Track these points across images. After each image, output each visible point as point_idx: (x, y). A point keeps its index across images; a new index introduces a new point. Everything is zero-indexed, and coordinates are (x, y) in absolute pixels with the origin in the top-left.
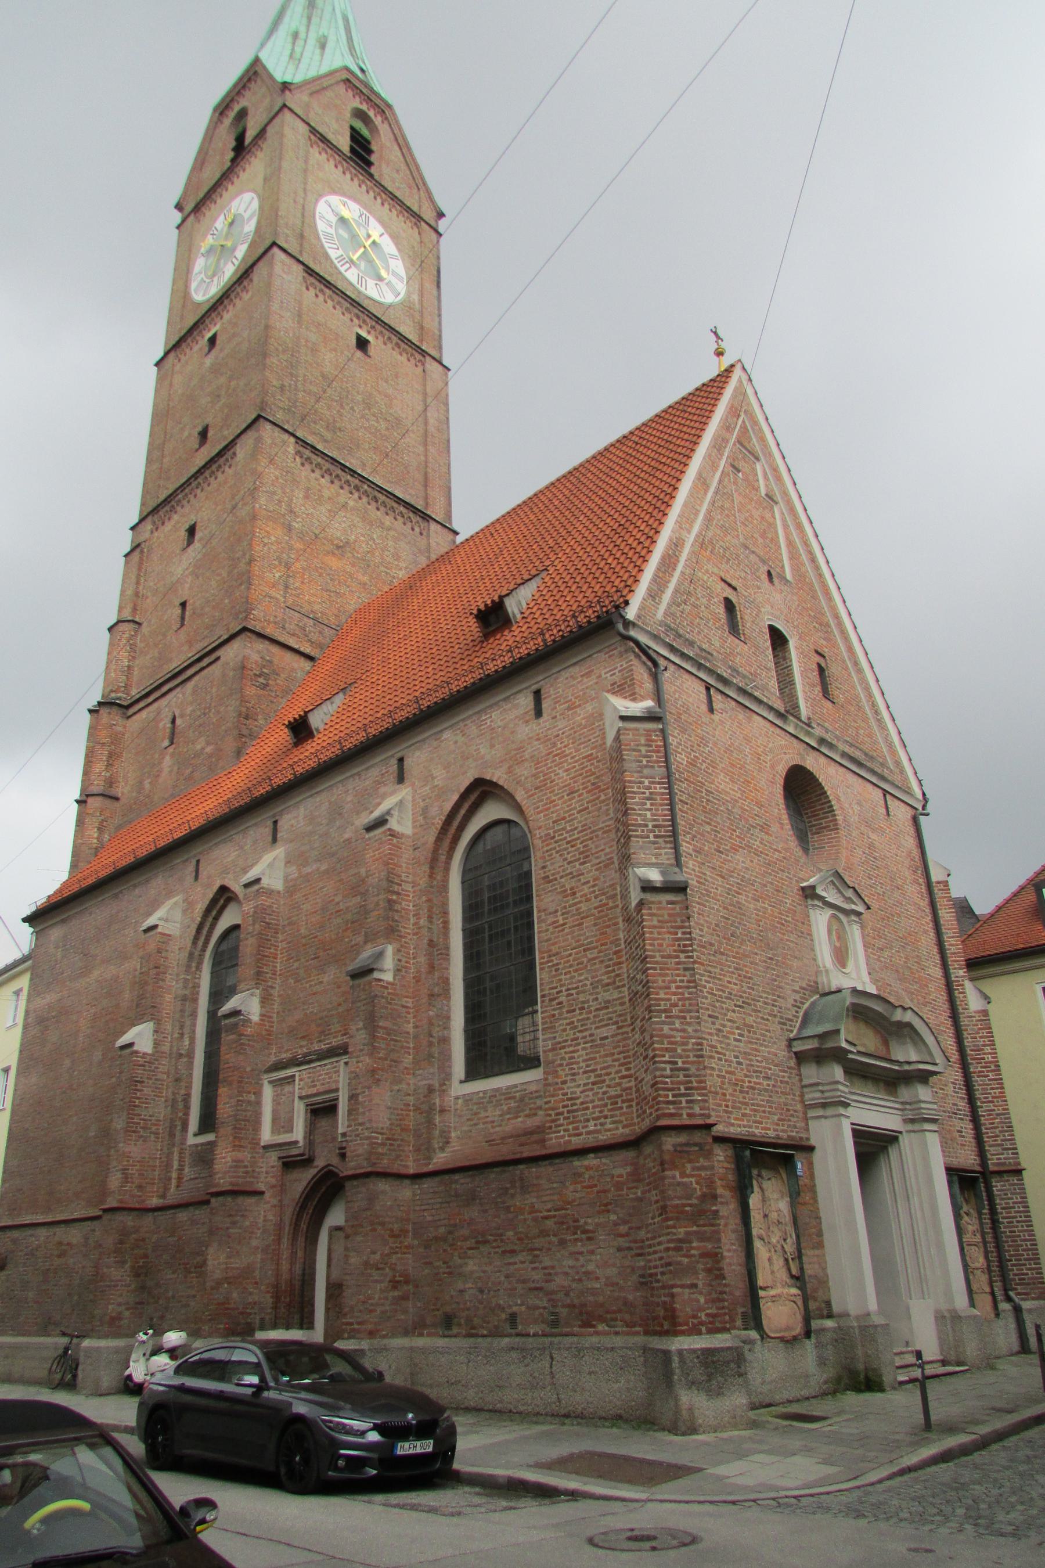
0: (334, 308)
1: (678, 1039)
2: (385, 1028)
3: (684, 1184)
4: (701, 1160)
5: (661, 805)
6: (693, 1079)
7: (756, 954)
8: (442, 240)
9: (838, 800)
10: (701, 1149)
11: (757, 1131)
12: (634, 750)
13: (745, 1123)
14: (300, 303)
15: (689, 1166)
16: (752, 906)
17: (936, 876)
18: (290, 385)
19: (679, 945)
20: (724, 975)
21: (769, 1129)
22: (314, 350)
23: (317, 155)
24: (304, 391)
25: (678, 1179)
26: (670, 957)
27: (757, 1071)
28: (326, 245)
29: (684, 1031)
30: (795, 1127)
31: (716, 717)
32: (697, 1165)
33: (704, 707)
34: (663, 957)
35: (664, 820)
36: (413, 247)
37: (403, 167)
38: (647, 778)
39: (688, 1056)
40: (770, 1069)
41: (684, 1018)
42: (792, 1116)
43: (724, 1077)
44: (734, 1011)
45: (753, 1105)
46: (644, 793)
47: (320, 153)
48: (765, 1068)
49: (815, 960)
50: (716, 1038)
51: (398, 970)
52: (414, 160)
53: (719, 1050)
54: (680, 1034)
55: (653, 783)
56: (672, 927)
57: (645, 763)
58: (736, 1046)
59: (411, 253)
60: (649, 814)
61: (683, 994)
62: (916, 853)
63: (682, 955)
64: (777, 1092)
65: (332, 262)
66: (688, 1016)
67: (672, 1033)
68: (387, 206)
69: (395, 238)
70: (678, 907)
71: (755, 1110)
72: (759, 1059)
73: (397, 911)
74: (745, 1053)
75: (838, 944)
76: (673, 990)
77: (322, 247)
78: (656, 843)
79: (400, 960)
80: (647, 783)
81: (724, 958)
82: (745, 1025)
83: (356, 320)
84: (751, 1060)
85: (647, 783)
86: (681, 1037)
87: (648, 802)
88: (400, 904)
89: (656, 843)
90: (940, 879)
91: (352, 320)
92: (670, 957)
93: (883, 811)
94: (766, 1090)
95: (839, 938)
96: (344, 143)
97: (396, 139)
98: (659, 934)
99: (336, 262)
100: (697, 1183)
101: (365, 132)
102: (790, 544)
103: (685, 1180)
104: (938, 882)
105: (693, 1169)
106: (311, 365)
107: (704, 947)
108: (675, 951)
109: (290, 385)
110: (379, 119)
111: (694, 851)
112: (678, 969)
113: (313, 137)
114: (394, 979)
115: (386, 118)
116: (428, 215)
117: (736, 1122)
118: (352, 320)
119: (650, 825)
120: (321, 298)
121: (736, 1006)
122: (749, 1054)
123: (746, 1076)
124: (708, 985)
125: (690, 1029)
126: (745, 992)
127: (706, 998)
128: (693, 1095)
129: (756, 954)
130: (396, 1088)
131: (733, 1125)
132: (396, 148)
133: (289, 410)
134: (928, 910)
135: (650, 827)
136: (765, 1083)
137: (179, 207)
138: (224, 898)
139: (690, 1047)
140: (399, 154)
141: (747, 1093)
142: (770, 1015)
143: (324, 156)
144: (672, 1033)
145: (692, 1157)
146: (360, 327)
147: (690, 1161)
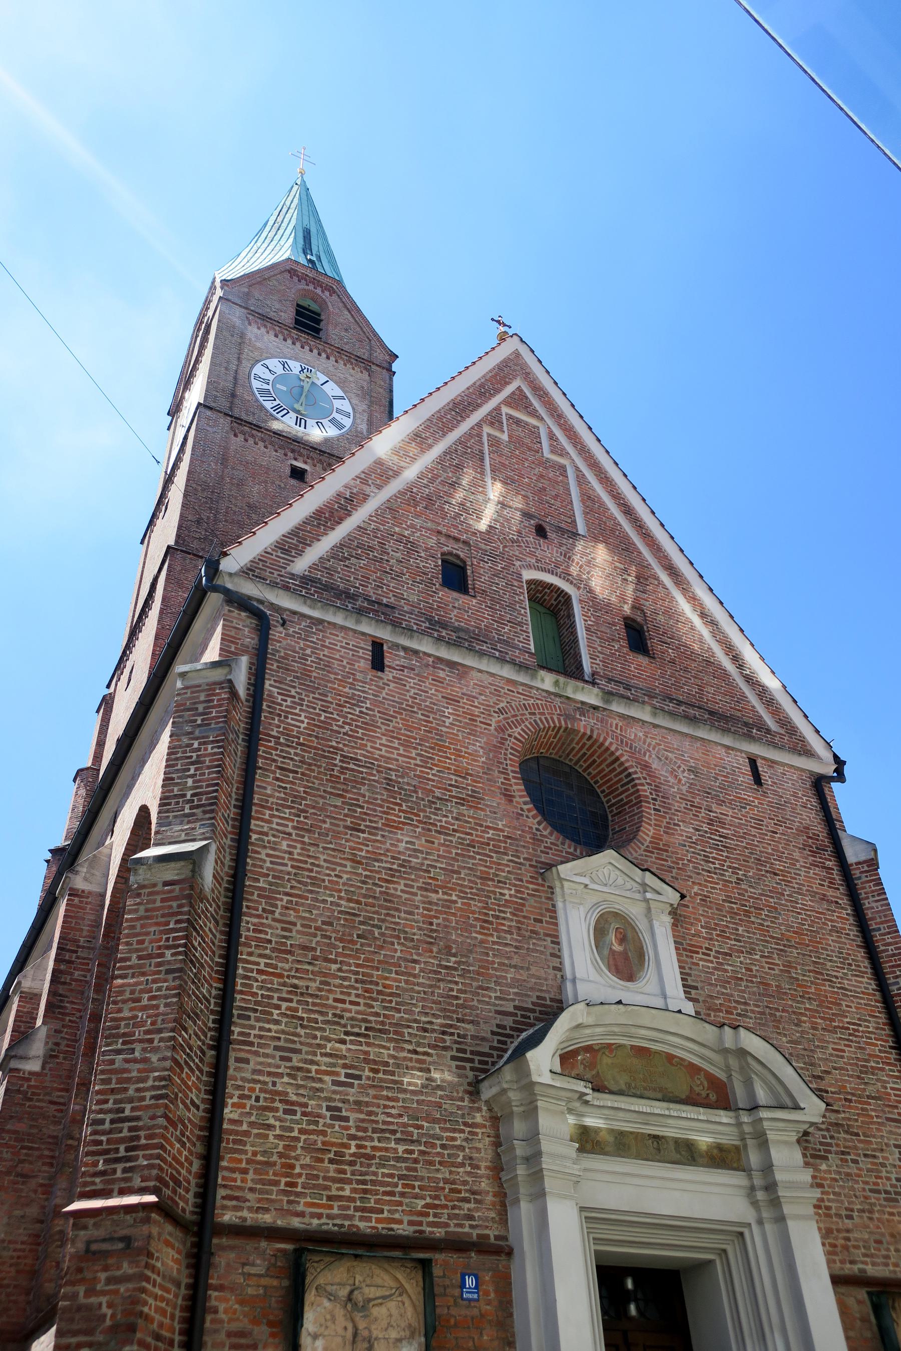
0: (266, 447)
1: (135, 1074)
2: (15, 1132)
3: (89, 1308)
4: (125, 1265)
5: (208, 767)
6: (142, 1133)
7: (415, 962)
8: (395, 378)
9: (646, 766)
10: (128, 1246)
11: (362, 1225)
12: (189, 710)
13: (335, 1211)
14: (226, 448)
15: (103, 1276)
16: (419, 898)
17: (852, 855)
18: (208, 518)
19: (167, 939)
20: (330, 991)
21: (400, 1222)
22: (240, 484)
23: (256, 330)
24: (226, 521)
25: (82, 1299)
26: (150, 956)
27: (383, 1131)
28: (261, 399)
29: (145, 1060)
30: (470, 1217)
31: (388, 674)
32: (119, 1273)
33: (364, 664)
34: (140, 958)
35: (208, 786)
36: (363, 387)
37: (354, 326)
38: (196, 739)
39: (143, 1099)
40: (420, 1127)
41: (151, 1041)
42: (466, 1200)
43: (297, 1139)
44: (343, 1042)
45: (364, 1182)
46: (191, 757)
47: (259, 328)
48: (405, 1125)
49: (560, 970)
50: (286, 1079)
51: (51, 1056)
52: (364, 318)
53: (294, 1098)
54: (138, 1066)
55: (205, 743)
56: (163, 916)
57: (199, 722)
58: (334, 1092)
59: (359, 392)
60: (190, 782)
61: (157, 1007)
62: (819, 828)
63: (168, 953)
64: (431, 1163)
65: (267, 411)
66: (156, 1037)
67: (127, 1066)
68: (332, 359)
69: (341, 383)
70: (177, 887)
71: (365, 1191)
72: (393, 1111)
73: (64, 983)
74: (358, 1103)
75: (617, 948)
76: (145, 1002)
77: (257, 400)
78: (193, 815)
79: (57, 1044)
80: (196, 745)
81: (334, 967)
82: (367, 1061)
83: (290, 454)
84: (370, 1113)
85: (196, 745)
86: (139, 1071)
87: (192, 768)
88: (72, 974)
89: (193, 815)
90: (862, 858)
91: (286, 455)
92: (150, 956)
93: (749, 779)
94: (398, 1159)
95: (622, 940)
96: (288, 316)
97: (345, 306)
98: (142, 926)
99: (272, 411)
100: (110, 1306)
101: (314, 307)
102: (589, 498)
103: (93, 1300)
104: (858, 863)
105: (109, 1281)
106: (236, 498)
107: (290, 952)
108: (159, 948)
109: (208, 518)
110: (327, 293)
111: (294, 828)
112: (159, 972)
113: (251, 317)
114: (43, 1067)
115: (334, 292)
116: (379, 356)
117: (309, 1210)
118: (286, 455)
119: (189, 794)
120: (251, 441)
121: (347, 1033)
122: (367, 1104)
123: (353, 1137)
124: (284, 1005)
125: (154, 1058)
126: (377, 1014)
127: (277, 1022)
128: (136, 1158)
129: (415, 962)
130: (18, 1213)
131: (301, 1214)
132: (346, 312)
133: (205, 539)
134: (844, 901)
135: (188, 797)
136: (401, 1148)
137: (168, 414)
138: (171, 1034)
139: (150, 1083)
140: (349, 316)
141: (352, 1163)
142: (434, 1047)
143: (263, 330)
144: (127, 1066)
145: (110, 1261)
146: (296, 459)
147: (106, 1269)
